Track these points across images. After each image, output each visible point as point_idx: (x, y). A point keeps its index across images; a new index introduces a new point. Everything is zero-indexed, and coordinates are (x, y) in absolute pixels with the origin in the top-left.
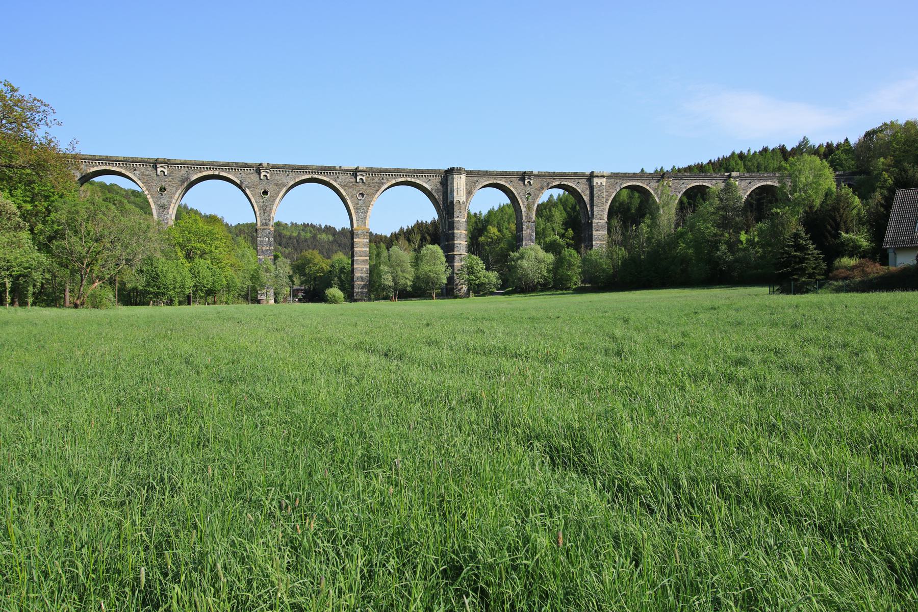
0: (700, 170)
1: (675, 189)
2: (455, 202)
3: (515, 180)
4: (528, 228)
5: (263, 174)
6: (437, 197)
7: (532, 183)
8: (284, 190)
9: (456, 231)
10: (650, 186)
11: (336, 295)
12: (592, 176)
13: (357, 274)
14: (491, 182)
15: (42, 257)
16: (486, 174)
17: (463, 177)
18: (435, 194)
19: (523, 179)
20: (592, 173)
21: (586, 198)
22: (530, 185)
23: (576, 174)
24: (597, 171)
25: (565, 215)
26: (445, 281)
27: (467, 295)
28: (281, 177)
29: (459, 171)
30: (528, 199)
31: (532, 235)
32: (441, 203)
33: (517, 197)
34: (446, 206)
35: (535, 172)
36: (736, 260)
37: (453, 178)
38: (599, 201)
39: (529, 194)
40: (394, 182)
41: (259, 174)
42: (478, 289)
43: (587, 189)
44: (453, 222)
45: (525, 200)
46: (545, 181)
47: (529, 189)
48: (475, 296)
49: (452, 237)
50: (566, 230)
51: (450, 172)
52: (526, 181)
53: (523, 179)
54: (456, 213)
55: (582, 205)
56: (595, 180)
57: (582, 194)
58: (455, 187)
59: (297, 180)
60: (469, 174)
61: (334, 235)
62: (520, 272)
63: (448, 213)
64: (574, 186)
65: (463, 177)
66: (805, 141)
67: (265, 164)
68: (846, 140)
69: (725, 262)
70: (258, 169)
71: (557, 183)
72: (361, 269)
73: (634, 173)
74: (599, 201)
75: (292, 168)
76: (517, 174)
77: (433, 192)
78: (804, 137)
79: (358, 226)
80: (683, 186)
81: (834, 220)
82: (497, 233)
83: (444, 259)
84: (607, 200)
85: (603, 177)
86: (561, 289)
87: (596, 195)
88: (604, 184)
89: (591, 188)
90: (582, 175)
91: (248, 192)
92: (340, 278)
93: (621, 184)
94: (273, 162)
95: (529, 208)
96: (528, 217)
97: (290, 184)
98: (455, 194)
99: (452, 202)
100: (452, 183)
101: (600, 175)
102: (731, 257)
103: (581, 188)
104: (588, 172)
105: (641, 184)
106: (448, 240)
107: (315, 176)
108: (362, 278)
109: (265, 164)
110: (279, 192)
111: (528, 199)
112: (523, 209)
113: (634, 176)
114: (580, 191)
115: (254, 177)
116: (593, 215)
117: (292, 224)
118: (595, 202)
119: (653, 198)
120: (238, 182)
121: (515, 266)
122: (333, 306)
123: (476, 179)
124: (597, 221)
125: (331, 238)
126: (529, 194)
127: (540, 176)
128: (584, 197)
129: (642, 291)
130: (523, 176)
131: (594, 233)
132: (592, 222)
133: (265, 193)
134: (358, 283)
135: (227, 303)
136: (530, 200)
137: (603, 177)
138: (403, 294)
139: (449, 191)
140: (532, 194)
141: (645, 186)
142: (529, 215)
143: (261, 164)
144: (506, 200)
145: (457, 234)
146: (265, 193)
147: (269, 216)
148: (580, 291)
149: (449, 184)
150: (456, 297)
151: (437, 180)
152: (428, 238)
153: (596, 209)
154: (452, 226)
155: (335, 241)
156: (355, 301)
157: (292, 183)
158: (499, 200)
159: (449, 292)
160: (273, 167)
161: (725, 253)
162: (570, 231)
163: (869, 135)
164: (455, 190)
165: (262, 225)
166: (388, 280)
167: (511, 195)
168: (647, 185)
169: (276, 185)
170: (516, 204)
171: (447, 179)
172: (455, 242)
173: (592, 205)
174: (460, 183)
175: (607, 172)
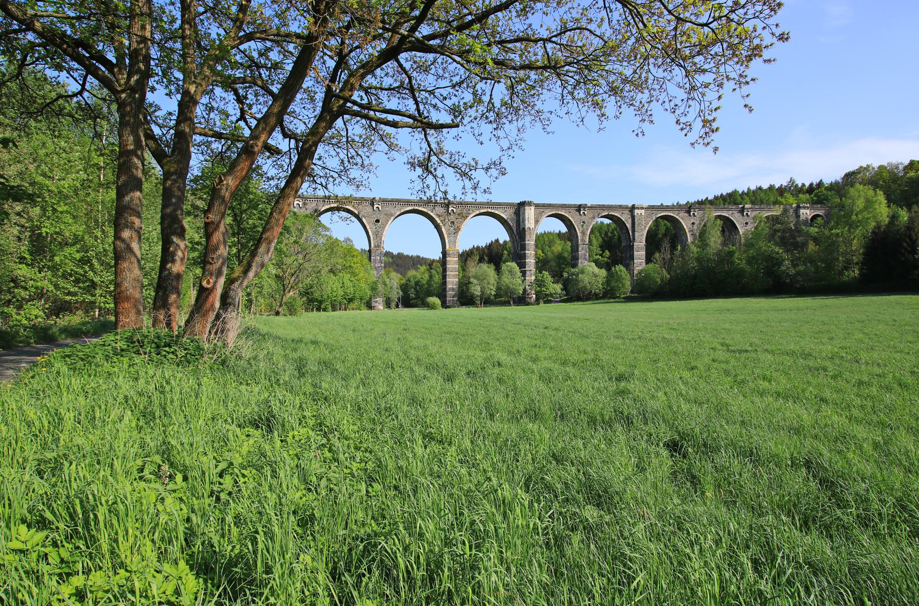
3: (573, 211)
4: (583, 249)
5: (376, 206)
8: (392, 218)
9: (527, 252)
10: (681, 217)
11: (436, 303)
12: (633, 208)
13: (449, 286)
14: (554, 212)
16: (550, 206)
17: (533, 208)
19: (579, 211)
20: (634, 205)
21: (629, 226)
23: (620, 207)
24: (637, 204)
25: (600, 240)
26: (521, 292)
27: (537, 302)
28: (390, 209)
29: (530, 204)
30: (582, 226)
32: (515, 229)
34: (518, 232)
35: (589, 205)
36: (799, 273)
37: (524, 210)
39: (584, 222)
40: (478, 212)
41: (373, 206)
42: (544, 298)
44: (525, 244)
46: (596, 212)
47: (583, 218)
49: (524, 256)
50: (603, 251)
51: (522, 204)
53: (579, 211)
54: (527, 238)
55: (624, 231)
56: (636, 211)
58: (527, 217)
59: (402, 211)
60: (537, 206)
61: (392, 258)
62: (581, 285)
63: (520, 238)
65: (533, 208)
66: (792, 181)
67: (377, 198)
69: (788, 274)
70: (372, 202)
71: (606, 213)
72: (452, 281)
75: (399, 201)
76: (575, 206)
77: (508, 220)
81: (911, 238)
82: (542, 254)
83: (520, 274)
84: (645, 227)
85: (642, 208)
86: (613, 298)
88: (643, 214)
89: (633, 217)
90: (626, 207)
91: (364, 220)
92: (415, 289)
94: (384, 196)
95: (583, 233)
96: (583, 240)
97: (397, 214)
98: (526, 222)
99: (524, 229)
100: (524, 213)
102: (793, 271)
103: (625, 218)
104: (630, 205)
105: (672, 215)
106: (520, 259)
107: (416, 208)
108: (453, 289)
109: (377, 198)
110: (388, 221)
111: (582, 226)
113: (667, 208)
115: (369, 209)
116: (634, 239)
117: (362, 250)
118: (636, 229)
119: (650, 228)
120: (357, 212)
121: (577, 280)
122: (432, 311)
123: (542, 210)
125: (391, 260)
126: (584, 222)
127: (592, 207)
129: (893, 298)
130: (579, 208)
131: (635, 253)
132: (633, 245)
133: (377, 221)
134: (450, 293)
136: (585, 227)
137: (642, 208)
138: (488, 302)
139: (521, 220)
142: (583, 237)
143: (374, 198)
144: (564, 229)
146: (377, 221)
147: (381, 239)
148: (629, 299)
150: (528, 304)
151: (512, 210)
152: (486, 258)
153: (637, 234)
154: (524, 247)
155: (394, 262)
156: (448, 307)
157: (399, 213)
158: (559, 227)
159: (522, 300)
160: (384, 201)
161: (788, 268)
162: (607, 253)
165: (375, 247)
166: (476, 290)
169: (386, 214)
170: (573, 230)
171: (519, 211)
173: (633, 231)
174: (530, 213)
175: (645, 205)
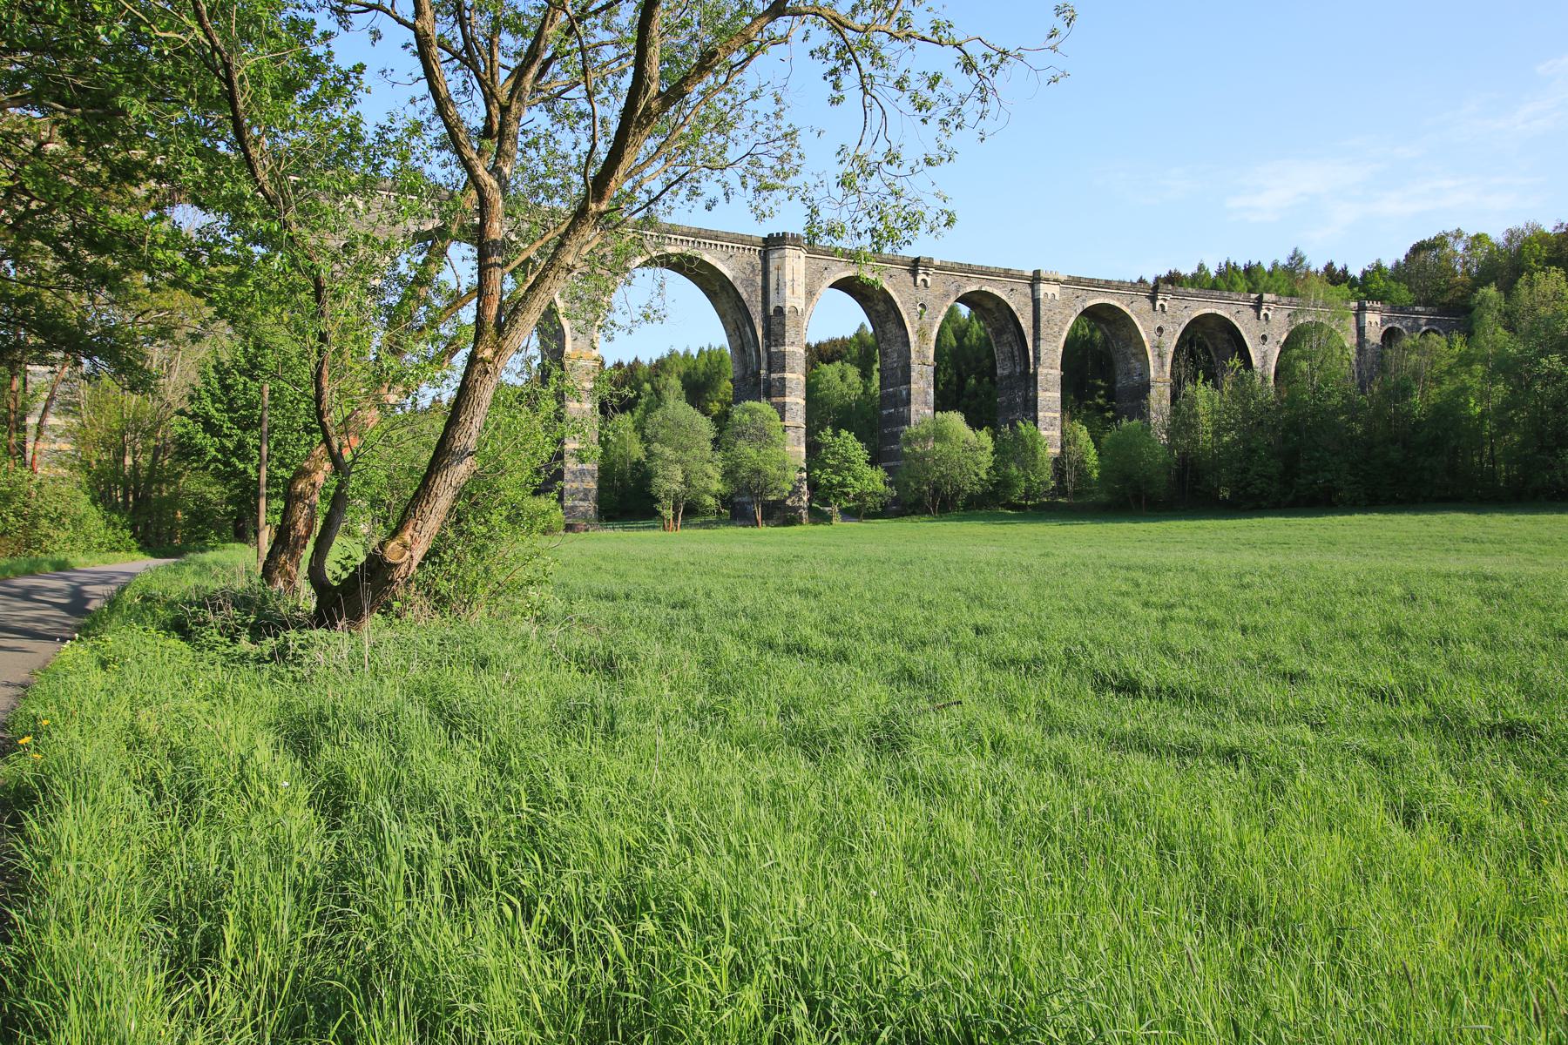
0: (1229, 279)
1: (1173, 317)
2: (787, 310)
6: (745, 296)
7: (929, 284)
12: (1036, 279)
15: (909, 252)
18: (741, 290)
20: (1037, 272)
21: (1026, 323)
22: (926, 285)
23: (1007, 273)
31: (927, 393)
33: (902, 310)
37: (783, 257)
38: (1049, 331)
43: (1026, 305)
45: (916, 319)
47: (922, 294)
48: (843, 521)
52: (919, 278)
57: (1018, 315)
58: (788, 278)
64: (1004, 297)
68: (1201, 267)
73: (1107, 281)
74: (1049, 331)
78: (1296, 250)
79: (574, 349)
80: (1185, 313)
87: (1043, 319)
89: (1036, 303)
93: (1084, 300)
98: (788, 292)
101: (1051, 277)
105: (1117, 304)
112: (913, 338)
114: (1014, 308)
116: (1037, 358)
123: (823, 264)
124: (1045, 371)
128: (1021, 320)
135: (587, 530)
140: (929, 307)
141: (1124, 308)
145: (791, 380)
149: (772, 269)
163: (1418, 249)
164: (789, 284)
167: (881, 307)
168: (1128, 306)
170: (891, 327)
172: (787, 400)
173: (1037, 338)
